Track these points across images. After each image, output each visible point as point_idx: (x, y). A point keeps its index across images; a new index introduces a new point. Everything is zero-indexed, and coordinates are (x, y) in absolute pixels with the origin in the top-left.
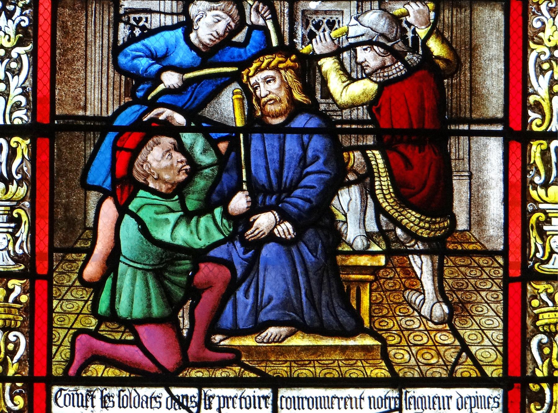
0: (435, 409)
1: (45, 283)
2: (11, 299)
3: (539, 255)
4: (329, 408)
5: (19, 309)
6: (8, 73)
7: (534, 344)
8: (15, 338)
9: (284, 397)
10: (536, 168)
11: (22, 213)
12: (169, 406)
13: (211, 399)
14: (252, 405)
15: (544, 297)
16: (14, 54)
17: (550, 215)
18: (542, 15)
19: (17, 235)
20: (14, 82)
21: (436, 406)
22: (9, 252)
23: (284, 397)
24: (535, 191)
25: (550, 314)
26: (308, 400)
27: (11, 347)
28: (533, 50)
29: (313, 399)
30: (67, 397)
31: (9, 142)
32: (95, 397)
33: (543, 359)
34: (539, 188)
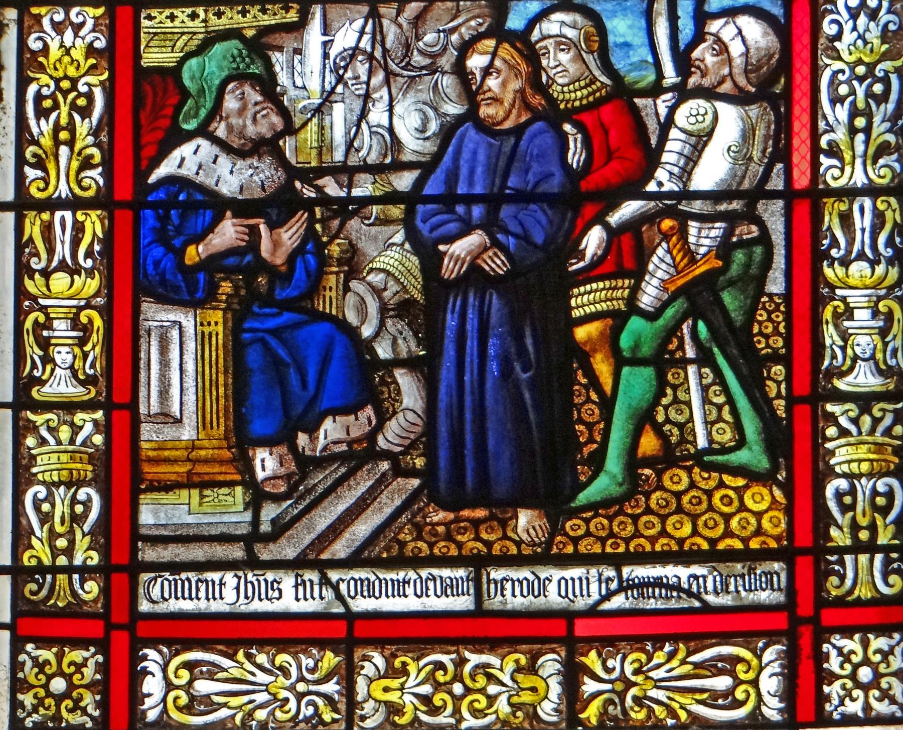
0: (406, 596)
1: (126, 414)
2: (79, 440)
3: (37, 373)
4: (400, 596)
5: (90, 455)
6: (870, 100)
7: (829, 491)
8: (887, 489)
9: (343, 581)
10: (833, 237)
11: (94, 314)
12: (439, 593)
13: (547, 582)
14: (173, 595)
15: (843, 421)
16: (83, 89)
17: (52, 315)
18: (839, 13)
19: (87, 348)
20: (83, 127)
21: (431, 592)
22: (877, 364)
23: (343, 581)
24: (32, 282)
25: (848, 448)
26: (521, 583)
27: (79, 509)
28: (827, 65)
29: (566, 581)
30: (166, 583)
31: (74, 215)
32: (224, 584)
33: (42, 523)
34: (836, 263)
